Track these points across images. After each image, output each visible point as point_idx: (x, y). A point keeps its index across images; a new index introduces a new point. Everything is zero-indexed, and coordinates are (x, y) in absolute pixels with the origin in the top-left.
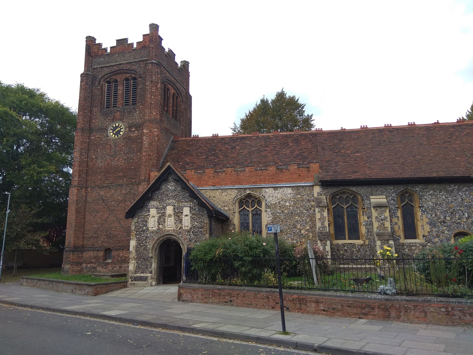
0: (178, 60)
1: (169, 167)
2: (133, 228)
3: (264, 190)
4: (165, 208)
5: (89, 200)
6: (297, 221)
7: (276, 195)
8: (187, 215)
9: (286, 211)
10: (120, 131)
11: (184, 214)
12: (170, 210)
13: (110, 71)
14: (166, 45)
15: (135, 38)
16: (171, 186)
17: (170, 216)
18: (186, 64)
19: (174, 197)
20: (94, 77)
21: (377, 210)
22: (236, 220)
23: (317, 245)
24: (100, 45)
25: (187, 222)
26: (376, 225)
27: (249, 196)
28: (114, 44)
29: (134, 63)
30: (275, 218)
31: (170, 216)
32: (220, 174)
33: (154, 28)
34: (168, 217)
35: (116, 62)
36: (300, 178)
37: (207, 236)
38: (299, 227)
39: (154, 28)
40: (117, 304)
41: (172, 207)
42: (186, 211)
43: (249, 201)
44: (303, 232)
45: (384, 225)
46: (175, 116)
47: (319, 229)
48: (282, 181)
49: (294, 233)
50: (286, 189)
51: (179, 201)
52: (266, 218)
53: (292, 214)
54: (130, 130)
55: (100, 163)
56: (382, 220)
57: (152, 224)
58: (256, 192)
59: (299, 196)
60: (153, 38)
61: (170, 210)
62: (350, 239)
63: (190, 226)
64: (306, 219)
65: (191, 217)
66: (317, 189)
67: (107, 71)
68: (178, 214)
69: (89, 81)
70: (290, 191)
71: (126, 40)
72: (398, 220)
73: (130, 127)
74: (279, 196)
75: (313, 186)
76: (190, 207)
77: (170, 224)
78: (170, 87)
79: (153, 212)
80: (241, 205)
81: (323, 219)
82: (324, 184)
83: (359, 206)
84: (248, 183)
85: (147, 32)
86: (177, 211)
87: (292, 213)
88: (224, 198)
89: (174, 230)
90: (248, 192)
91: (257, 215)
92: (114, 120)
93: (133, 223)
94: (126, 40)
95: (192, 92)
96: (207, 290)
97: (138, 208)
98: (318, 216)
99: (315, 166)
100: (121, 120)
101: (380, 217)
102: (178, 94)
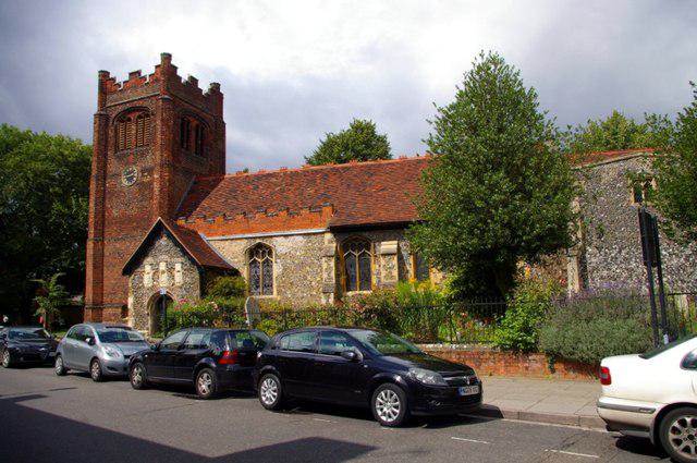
0: (204, 87)
1: (160, 222)
2: (130, 285)
4: (158, 264)
5: (106, 253)
7: (286, 245)
10: (132, 177)
12: (163, 266)
14: (184, 74)
15: (148, 70)
16: (163, 241)
17: (163, 272)
18: (215, 88)
19: (167, 252)
20: (107, 118)
22: (245, 273)
24: (114, 79)
25: (179, 278)
26: (383, 273)
27: (260, 246)
28: (127, 78)
30: (285, 269)
31: (163, 272)
33: (167, 57)
39: (167, 57)
40: (675, 448)
42: (178, 267)
43: (259, 251)
46: (200, 151)
48: (293, 228)
50: (296, 237)
51: (171, 257)
52: (277, 270)
53: (302, 265)
54: (143, 176)
55: (115, 213)
57: (147, 280)
60: (167, 67)
61: (163, 266)
63: (182, 282)
66: (329, 236)
67: (120, 109)
68: (170, 269)
69: (103, 119)
70: (301, 238)
71: (139, 73)
73: (143, 172)
74: (290, 244)
75: (323, 233)
77: (163, 284)
79: (148, 268)
80: (251, 256)
81: (327, 271)
82: (333, 230)
85: (159, 62)
88: (231, 250)
90: (258, 241)
91: (268, 264)
92: (127, 163)
93: (130, 281)
94: (139, 73)
96: (274, 348)
97: (133, 266)
98: (325, 266)
99: (327, 210)
100: (134, 164)
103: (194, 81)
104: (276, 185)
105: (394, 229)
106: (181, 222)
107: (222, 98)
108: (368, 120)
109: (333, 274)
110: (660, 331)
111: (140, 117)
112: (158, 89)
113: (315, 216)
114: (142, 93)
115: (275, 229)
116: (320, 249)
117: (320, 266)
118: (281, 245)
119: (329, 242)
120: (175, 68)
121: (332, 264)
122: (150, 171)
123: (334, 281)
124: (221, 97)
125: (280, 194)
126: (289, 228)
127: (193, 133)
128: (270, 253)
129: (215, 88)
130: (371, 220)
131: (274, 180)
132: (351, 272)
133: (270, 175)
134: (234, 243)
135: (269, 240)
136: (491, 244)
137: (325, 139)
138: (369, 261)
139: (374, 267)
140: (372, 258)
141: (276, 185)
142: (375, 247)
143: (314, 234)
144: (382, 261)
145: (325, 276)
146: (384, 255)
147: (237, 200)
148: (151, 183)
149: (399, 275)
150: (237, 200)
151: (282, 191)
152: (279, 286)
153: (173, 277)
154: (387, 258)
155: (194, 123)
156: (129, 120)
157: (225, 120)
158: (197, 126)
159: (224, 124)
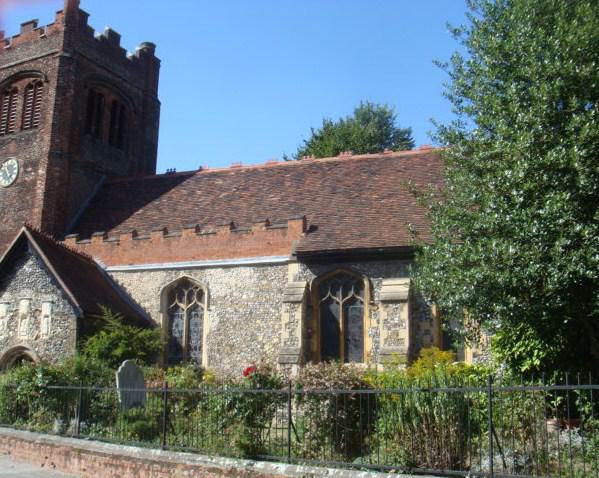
0: (132, 48)
1: (24, 232)
3: (208, 271)
6: (259, 329)
8: (46, 316)
9: (241, 310)
11: (43, 314)
13: (8, 75)
14: (99, 28)
18: (148, 51)
21: (387, 307)
23: (289, 374)
26: (384, 334)
27: (185, 283)
29: (41, 60)
31: (24, 317)
32: (142, 243)
34: (22, 319)
35: (17, 59)
36: (271, 248)
37: (74, 351)
38: (260, 339)
41: (27, 302)
42: (46, 309)
43: (181, 292)
44: (267, 347)
45: (398, 335)
47: (285, 343)
49: (253, 350)
53: (250, 316)
54: (25, 172)
56: (395, 325)
58: (196, 275)
59: (264, 282)
61: (23, 307)
62: (593, 384)
64: (274, 326)
65: (52, 319)
66: (295, 269)
68: (35, 313)
70: (248, 271)
71: (34, 23)
72: (431, 325)
74: (233, 282)
75: (286, 263)
76: (53, 302)
78: (105, 91)
82: (303, 257)
83: (365, 298)
84: (185, 259)
86: (33, 308)
87: (251, 313)
89: (29, 340)
90: (182, 274)
91: (194, 312)
95: (161, 96)
98: (285, 318)
99: (296, 226)
100: (15, 154)
101: (392, 319)
102: (125, 100)
103: (114, 37)
104: (222, 190)
105: (396, 259)
106: (70, 242)
107: (159, 66)
108: (382, 106)
109: (298, 333)
110: (30, 202)
111: (30, 86)
112: (57, 45)
113: (275, 236)
114: (35, 51)
115: (210, 256)
116: (280, 291)
117: (279, 318)
118: (217, 282)
119: (297, 278)
120: (85, 16)
121: (298, 314)
122: (34, 164)
123: (300, 344)
124: (156, 63)
125: (241, 202)
126: (234, 254)
127: (107, 112)
128: (200, 295)
129: (148, 51)
130: (366, 243)
131: (220, 182)
132: (329, 336)
133: (215, 175)
134: (146, 277)
135: (199, 272)
136: (564, 163)
137: (319, 127)
138: (361, 311)
139: (369, 324)
140: (366, 309)
141: (222, 190)
142: (371, 288)
143: (271, 265)
144: (383, 313)
145: (285, 335)
146: (386, 302)
147: (160, 211)
148: (34, 183)
149: (412, 337)
150: (160, 211)
151: (230, 199)
152: (211, 350)
153: (37, 325)
154: (392, 306)
155: (111, 98)
156: (15, 91)
157: (160, 98)
158: (114, 103)
159: (159, 103)
